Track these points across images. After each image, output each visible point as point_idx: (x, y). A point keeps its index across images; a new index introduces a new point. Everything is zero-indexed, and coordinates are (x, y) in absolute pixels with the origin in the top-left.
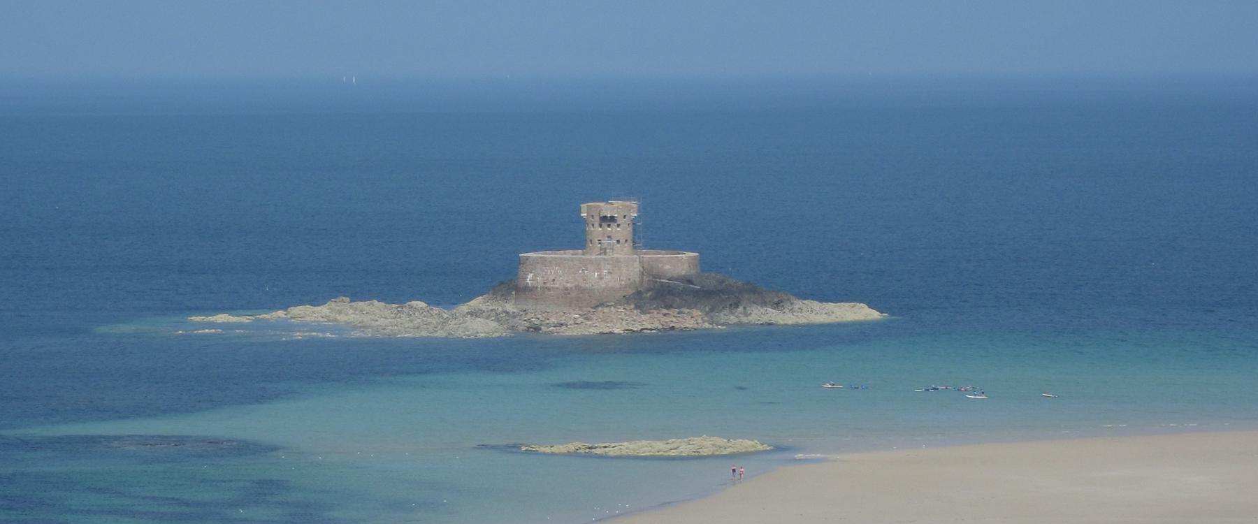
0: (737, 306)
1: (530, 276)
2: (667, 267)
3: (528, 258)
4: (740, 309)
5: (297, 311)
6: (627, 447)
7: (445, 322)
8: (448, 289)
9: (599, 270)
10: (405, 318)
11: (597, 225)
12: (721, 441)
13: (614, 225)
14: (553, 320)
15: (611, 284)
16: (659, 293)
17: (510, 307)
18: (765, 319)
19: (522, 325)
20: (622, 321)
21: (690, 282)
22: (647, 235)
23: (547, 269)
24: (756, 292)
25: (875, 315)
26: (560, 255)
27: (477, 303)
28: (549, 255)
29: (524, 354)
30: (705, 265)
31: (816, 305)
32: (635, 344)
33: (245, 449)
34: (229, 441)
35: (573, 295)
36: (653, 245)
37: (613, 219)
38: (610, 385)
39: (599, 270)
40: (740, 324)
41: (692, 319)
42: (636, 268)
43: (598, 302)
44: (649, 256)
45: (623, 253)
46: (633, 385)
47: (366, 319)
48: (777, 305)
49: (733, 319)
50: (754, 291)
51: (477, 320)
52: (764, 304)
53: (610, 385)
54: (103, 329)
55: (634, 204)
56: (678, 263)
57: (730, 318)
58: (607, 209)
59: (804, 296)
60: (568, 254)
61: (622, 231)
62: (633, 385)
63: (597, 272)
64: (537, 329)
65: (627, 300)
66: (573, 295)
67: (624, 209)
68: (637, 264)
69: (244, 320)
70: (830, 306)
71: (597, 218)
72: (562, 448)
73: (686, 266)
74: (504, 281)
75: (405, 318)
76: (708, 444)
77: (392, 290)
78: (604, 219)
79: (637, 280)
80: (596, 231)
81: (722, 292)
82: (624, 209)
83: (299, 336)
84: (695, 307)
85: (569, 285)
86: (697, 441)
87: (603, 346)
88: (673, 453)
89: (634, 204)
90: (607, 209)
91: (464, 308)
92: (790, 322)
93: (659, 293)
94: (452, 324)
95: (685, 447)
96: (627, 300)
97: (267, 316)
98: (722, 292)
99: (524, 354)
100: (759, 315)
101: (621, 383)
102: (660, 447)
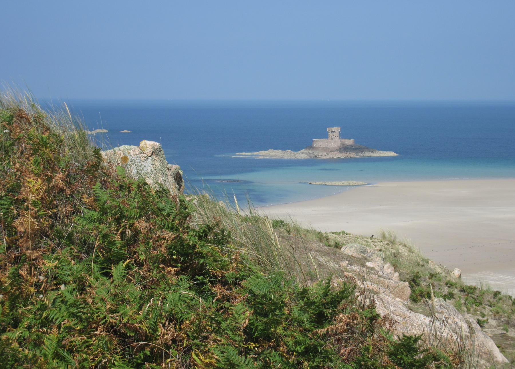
5: (261, 152)
6: (333, 183)
7: (295, 155)
8: (296, 149)
10: (286, 154)
12: (354, 182)
14: (320, 155)
16: (344, 149)
17: (310, 152)
18: (369, 155)
19: (313, 156)
20: (336, 155)
22: (342, 135)
23: (319, 143)
24: (368, 149)
25: (395, 154)
26: (322, 140)
27: (303, 151)
28: (319, 140)
29: (313, 162)
31: (382, 152)
32: (339, 161)
33: (246, 182)
36: (345, 138)
37: (334, 131)
38: (330, 170)
40: (364, 156)
41: (352, 155)
43: (331, 151)
44: (343, 140)
45: (337, 139)
46: (333, 170)
47: (277, 154)
48: (372, 152)
49: (362, 155)
50: (367, 148)
51: (303, 155)
52: (369, 151)
53: (330, 170)
54: (217, 156)
55: (339, 128)
56: (349, 142)
57: (361, 155)
58: (333, 129)
59: (379, 150)
60: (324, 139)
61: (337, 134)
62: (337, 170)
63: (330, 144)
64: (316, 157)
65: (337, 150)
67: (337, 129)
69: (249, 154)
70: (385, 152)
72: (318, 183)
74: (310, 146)
75: (286, 154)
76: (351, 182)
77: (284, 148)
78: (332, 131)
80: (331, 134)
82: (337, 129)
83: (261, 158)
86: (349, 182)
87: (332, 161)
88: (343, 185)
89: (339, 128)
90: (333, 129)
91: (300, 152)
94: (296, 155)
95: (346, 183)
96: (337, 150)
97: (219, 156)
99: (313, 162)
100: (368, 154)
102: (340, 183)
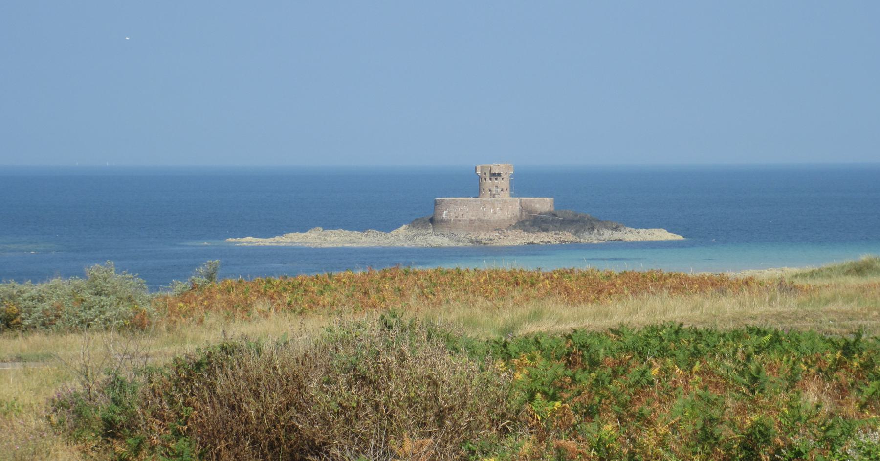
0: (593, 230)
1: (445, 212)
2: (537, 206)
3: (443, 201)
4: (596, 231)
9: (494, 208)
11: (488, 179)
13: (499, 179)
15: (502, 217)
16: (534, 222)
20: (519, 239)
21: (555, 215)
25: (680, 237)
30: (556, 204)
34: (737, 336)
35: (476, 224)
37: (499, 174)
39: (494, 208)
42: (517, 207)
56: (543, 205)
66: (476, 224)
68: (518, 204)
70: (642, 231)
71: (488, 174)
73: (549, 206)
79: (518, 214)
81: (577, 221)
84: (565, 230)
85: (473, 218)
92: (632, 239)
93: (534, 222)
98: (577, 221)
101: (848, 272)
